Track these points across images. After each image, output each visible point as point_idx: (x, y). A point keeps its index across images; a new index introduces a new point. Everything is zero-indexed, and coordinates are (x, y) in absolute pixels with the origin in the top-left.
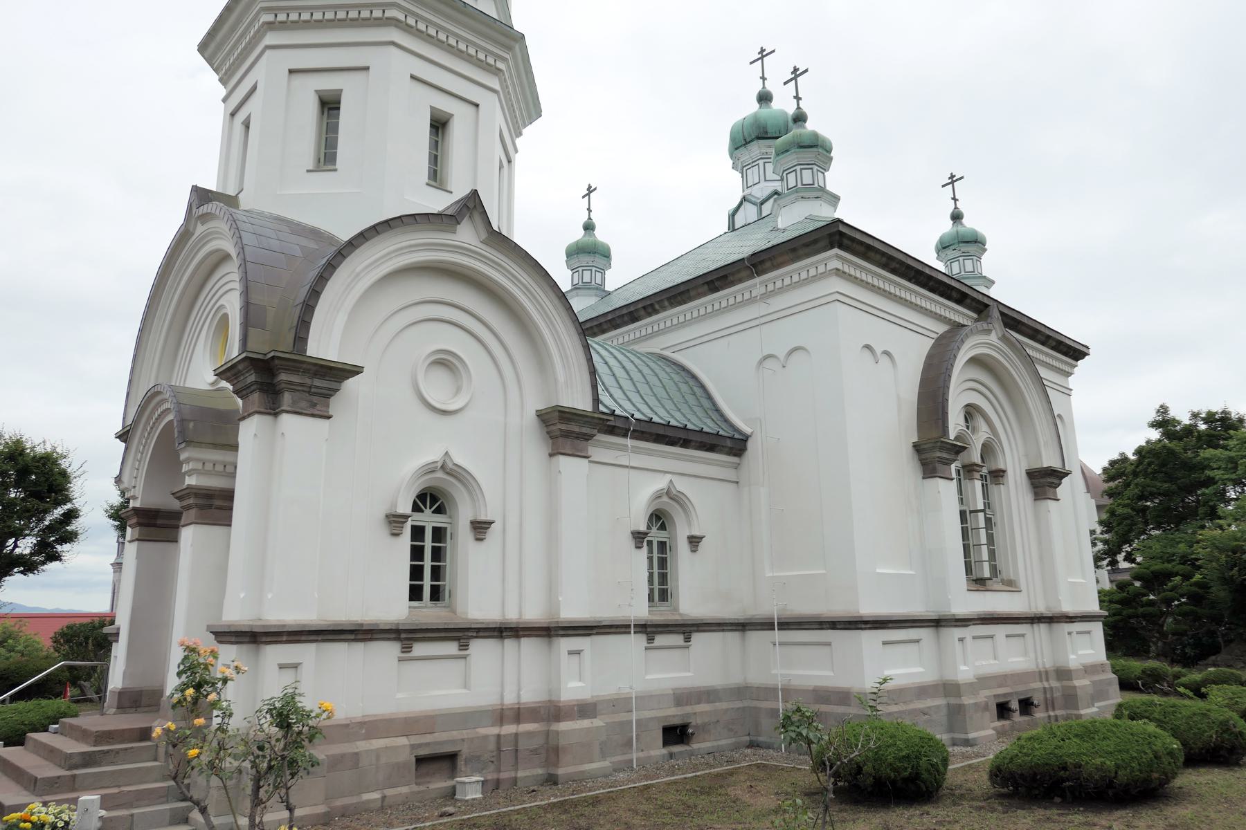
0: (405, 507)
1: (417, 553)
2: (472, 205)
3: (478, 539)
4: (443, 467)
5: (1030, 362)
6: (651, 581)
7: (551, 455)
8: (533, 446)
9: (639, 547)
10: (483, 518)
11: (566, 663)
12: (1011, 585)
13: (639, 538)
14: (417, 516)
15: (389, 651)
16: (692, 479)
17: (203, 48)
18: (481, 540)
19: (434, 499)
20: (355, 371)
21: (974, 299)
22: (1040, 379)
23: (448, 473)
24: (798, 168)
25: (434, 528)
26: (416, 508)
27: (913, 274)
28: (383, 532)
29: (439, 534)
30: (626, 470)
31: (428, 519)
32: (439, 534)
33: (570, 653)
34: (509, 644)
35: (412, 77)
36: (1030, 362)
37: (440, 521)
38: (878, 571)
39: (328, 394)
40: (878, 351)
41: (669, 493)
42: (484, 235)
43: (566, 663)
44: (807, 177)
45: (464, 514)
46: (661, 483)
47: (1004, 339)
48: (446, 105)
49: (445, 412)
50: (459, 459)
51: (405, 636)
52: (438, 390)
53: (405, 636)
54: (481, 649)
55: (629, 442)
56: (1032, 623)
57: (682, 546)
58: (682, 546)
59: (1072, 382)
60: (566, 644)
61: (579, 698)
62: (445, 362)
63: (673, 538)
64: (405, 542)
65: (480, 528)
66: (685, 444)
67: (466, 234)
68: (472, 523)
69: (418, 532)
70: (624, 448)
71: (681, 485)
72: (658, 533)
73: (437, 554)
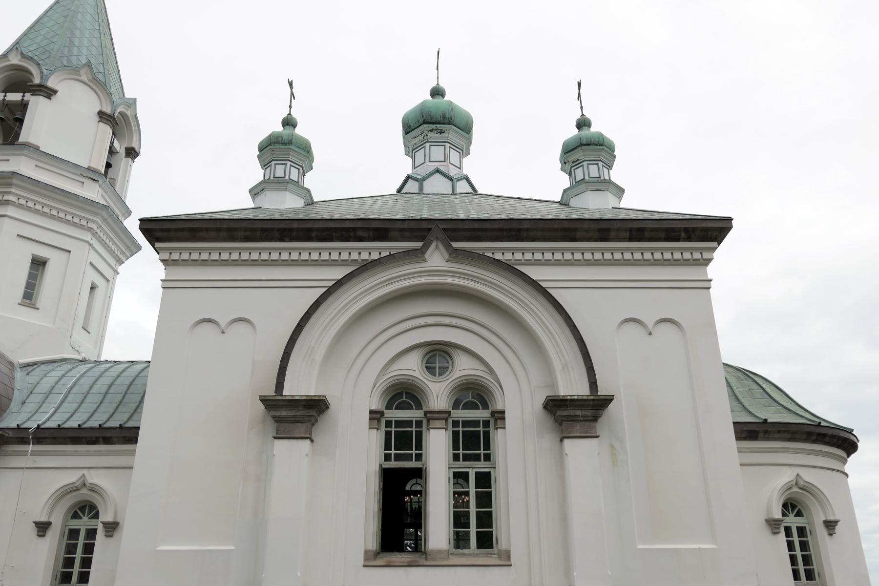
0: (778, 515)
1: (790, 546)
3: (39, 536)
4: (796, 484)
5: (509, 269)
9: (775, 533)
10: (831, 518)
13: (773, 525)
16: (115, 471)
18: (111, 536)
19: (794, 507)
21: (318, 230)
22: (534, 284)
23: (800, 488)
24: (289, 163)
25: (797, 527)
26: (784, 515)
27: (258, 234)
28: (766, 532)
29: (801, 531)
30: (21, 471)
31: (793, 521)
32: (801, 531)
35: (91, 264)
36: (509, 269)
38: (640, 547)
40: (650, 322)
41: (797, 482)
44: (594, 171)
45: (818, 518)
46: (786, 476)
47: (456, 255)
57: (821, 531)
58: (821, 531)
59: (711, 270)
63: (811, 523)
64: (782, 537)
66: (107, 441)
68: (767, 521)
69: (788, 530)
70: (24, 453)
71: (94, 478)
73: (804, 546)
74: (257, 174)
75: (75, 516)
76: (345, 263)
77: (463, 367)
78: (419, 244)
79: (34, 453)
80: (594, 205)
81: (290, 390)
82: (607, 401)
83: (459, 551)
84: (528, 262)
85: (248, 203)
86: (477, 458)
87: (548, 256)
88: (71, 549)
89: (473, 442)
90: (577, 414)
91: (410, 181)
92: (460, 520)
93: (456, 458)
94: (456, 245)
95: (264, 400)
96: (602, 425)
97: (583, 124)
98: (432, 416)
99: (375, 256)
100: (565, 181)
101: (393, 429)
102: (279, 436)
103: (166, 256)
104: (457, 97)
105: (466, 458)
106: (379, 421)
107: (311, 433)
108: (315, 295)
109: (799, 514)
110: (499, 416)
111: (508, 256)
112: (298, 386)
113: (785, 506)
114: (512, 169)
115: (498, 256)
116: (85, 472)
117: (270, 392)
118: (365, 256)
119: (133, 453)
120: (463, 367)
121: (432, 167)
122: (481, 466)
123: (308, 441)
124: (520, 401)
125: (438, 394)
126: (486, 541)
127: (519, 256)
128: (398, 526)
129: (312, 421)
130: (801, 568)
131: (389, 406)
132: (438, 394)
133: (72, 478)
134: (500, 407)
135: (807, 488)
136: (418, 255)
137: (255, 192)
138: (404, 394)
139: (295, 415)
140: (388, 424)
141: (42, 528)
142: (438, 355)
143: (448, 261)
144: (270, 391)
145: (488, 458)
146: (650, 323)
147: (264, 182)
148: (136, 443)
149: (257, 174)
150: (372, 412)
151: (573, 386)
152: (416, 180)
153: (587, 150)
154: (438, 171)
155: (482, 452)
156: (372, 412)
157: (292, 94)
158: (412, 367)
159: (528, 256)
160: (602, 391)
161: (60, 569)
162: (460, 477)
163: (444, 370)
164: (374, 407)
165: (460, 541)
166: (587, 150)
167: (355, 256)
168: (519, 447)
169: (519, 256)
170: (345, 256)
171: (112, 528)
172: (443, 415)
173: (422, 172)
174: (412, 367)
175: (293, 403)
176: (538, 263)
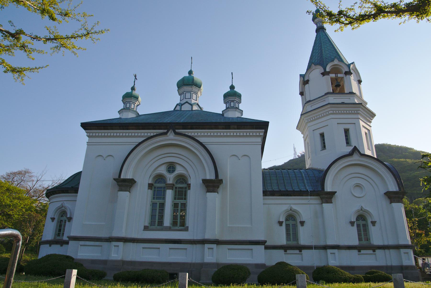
0: (282, 219)
1: (359, 231)
2: (355, 149)
4: (361, 209)
6: (64, 229)
7: (390, 203)
8: (385, 202)
10: (373, 220)
11: (113, 248)
12: (187, 229)
14: (358, 222)
15: (355, 252)
17: (297, 128)
20: (336, 192)
26: (357, 220)
31: (361, 222)
33: (115, 246)
34: (387, 251)
37: (364, 222)
39: (331, 198)
42: (359, 155)
43: (113, 248)
45: (369, 220)
48: (347, 127)
49: (360, 197)
50: (366, 208)
51: (359, 248)
52: (357, 193)
53: (285, 248)
54: (378, 252)
55: (309, 197)
56: (384, 249)
60: (207, 246)
61: (370, 265)
62: (358, 186)
64: (355, 228)
65: (374, 223)
67: (356, 157)
69: (358, 226)
71: (295, 207)
72: (291, 222)
74: (122, 106)
75: (62, 216)
76: (142, 137)
77: (179, 170)
78: (166, 131)
79: (311, 199)
80: (232, 115)
81: (122, 177)
82: (221, 181)
84: (199, 136)
85: (117, 116)
86: (182, 199)
90: (212, 185)
91: (178, 106)
92: (175, 218)
93: (154, 198)
94: (177, 131)
95: (114, 179)
96: (333, 200)
97: (232, 87)
98: (171, 187)
99: (152, 135)
100: (224, 107)
102: (208, 191)
103: (88, 135)
104: (197, 76)
105: (157, 198)
106: (152, 187)
107: (130, 189)
108: (134, 146)
110: (189, 186)
111: (193, 134)
112: (127, 175)
114: (211, 102)
115: (189, 134)
116: (62, 202)
117: (117, 177)
118: (149, 134)
119: (77, 196)
120: (179, 170)
121: (185, 101)
122: (183, 201)
123: (128, 192)
124: (195, 181)
125: (170, 178)
126: (183, 224)
127: (196, 134)
128: (156, 220)
129: (131, 187)
131: (176, 183)
132: (170, 178)
133: (59, 204)
134: (189, 183)
136: (165, 134)
137: (119, 112)
138: (160, 178)
139: (125, 184)
140: (176, 188)
142: (171, 167)
143: (174, 136)
144: (117, 177)
146: (105, 156)
147: (124, 109)
148: (77, 193)
149: (122, 106)
150: (149, 184)
151: (210, 176)
152: (179, 105)
153: (232, 97)
154: (187, 102)
156: (149, 184)
157: (136, 78)
158: (163, 170)
159: (199, 134)
160: (220, 178)
161: (57, 232)
162: (175, 205)
163: (173, 171)
164: (150, 183)
165: (174, 223)
166: (232, 97)
167: (146, 134)
168: (195, 194)
170: (143, 134)
171: (70, 219)
172: (171, 187)
173: (182, 102)
174: (163, 170)
175: (125, 180)
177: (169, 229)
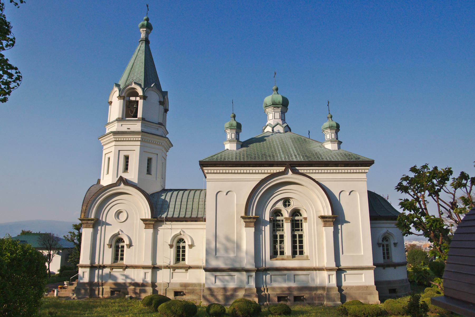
0: (380, 242)
9: (379, 247)
19: (386, 239)
26: (383, 241)
31: (385, 243)
32: (387, 245)
45: (392, 242)
57: (392, 246)
58: (392, 246)
62: (118, 213)
64: (381, 248)
66: (186, 221)
69: (383, 246)
73: (387, 250)
83: (210, 215)
84: (309, 173)
86: (299, 230)
87: (311, 171)
88: (178, 251)
89: (296, 225)
101: (300, 228)
109: (387, 241)
111: (305, 171)
113: (383, 239)
115: (302, 171)
118: (272, 172)
120: (294, 205)
122: (300, 233)
125: (286, 213)
126: (301, 253)
127: (308, 171)
130: (386, 255)
135: (390, 234)
141: (171, 246)
145: (302, 230)
155: (300, 228)
163: (289, 205)
165: (294, 253)
167: (269, 171)
169: (308, 171)
176: (312, 173)
177: (288, 259)
